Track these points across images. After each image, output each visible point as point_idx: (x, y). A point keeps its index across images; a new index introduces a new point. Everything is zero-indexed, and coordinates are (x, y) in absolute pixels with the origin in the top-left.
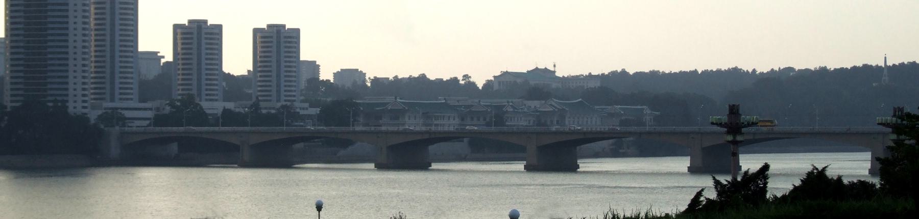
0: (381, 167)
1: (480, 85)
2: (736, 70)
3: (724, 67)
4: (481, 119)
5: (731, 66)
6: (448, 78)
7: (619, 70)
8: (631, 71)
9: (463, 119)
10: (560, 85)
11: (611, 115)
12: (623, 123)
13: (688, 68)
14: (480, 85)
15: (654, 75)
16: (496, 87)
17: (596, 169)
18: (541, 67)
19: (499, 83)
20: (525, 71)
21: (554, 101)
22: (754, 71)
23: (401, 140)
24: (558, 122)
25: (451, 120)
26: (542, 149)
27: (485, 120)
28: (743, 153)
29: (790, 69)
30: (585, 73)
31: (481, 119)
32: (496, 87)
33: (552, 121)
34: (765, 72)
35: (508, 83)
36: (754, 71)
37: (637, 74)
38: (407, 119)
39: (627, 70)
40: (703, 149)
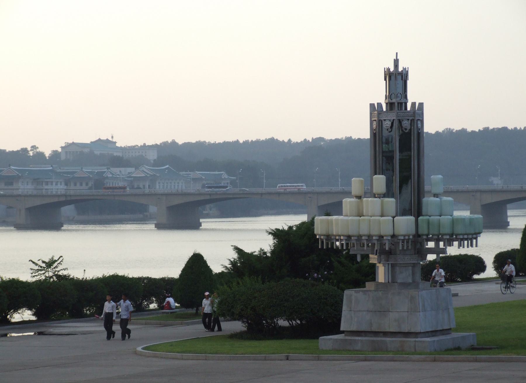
0: (160, 227)
1: (47, 154)
2: (272, 139)
3: (263, 138)
4: (84, 184)
5: (269, 137)
6: (264, 139)
7: (170, 141)
8: (469, 130)
9: (66, 184)
10: (120, 154)
11: (195, 180)
12: (204, 186)
13: (231, 139)
14: (47, 154)
15: (200, 145)
16: (63, 157)
17: (211, 227)
18: (104, 138)
19: (66, 152)
20: (89, 142)
21: (146, 168)
22: (290, 140)
23: (38, 202)
24: (149, 186)
25: (59, 185)
26: (171, 209)
27: (87, 184)
28: (511, 209)
29: (321, 139)
30: (140, 144)
31: (84, 184)
32: (63, 157)
33: (144, 186)
34: (299, 141)
35: (76, 154)
36: (290, 140)
37: (185, 144)
38: (20, 184)
39: (177, 141)
40: (482, 206)
